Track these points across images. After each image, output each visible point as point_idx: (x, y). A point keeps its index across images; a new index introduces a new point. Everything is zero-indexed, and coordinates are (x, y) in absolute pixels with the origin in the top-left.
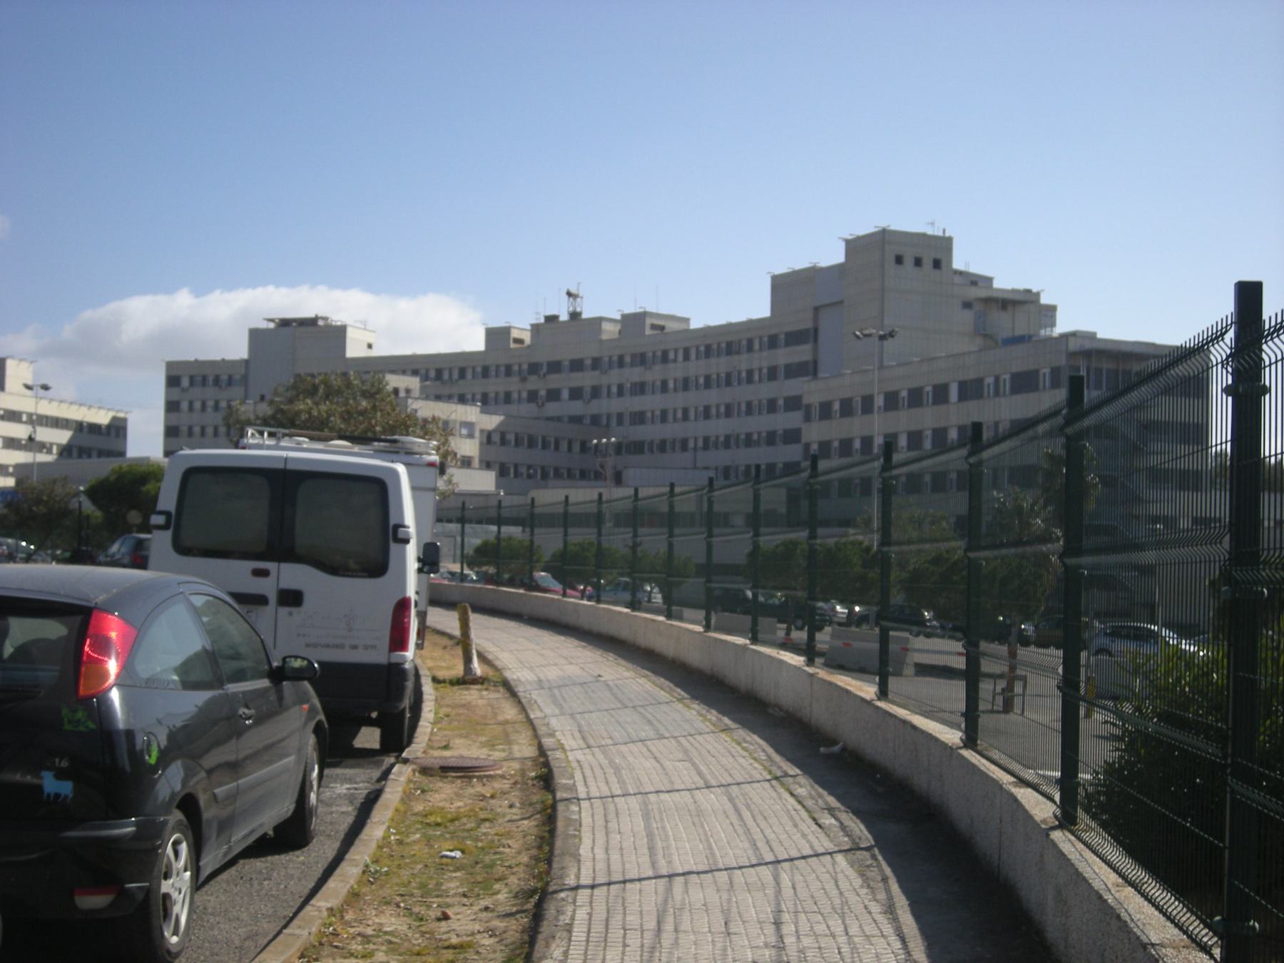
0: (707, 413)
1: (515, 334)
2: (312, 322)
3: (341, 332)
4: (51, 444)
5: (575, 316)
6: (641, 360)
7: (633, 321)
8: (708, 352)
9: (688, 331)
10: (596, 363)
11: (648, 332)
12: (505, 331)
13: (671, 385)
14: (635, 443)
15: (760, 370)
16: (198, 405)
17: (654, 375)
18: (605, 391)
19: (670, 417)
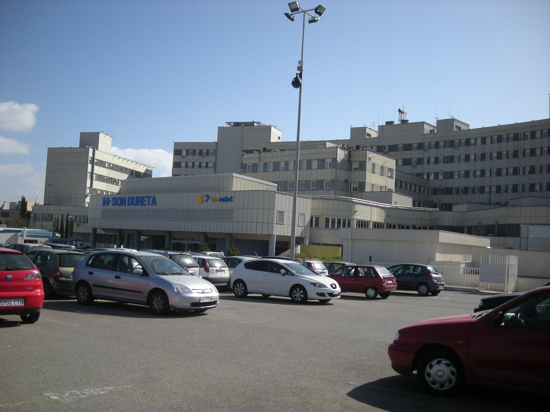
0: (499, 172)
1: (368, 131)
2: (252, 124)
3: (268, 129)
4: (119, 180)
5: (404, 122)
6: (451, 144)
7: (446, 125)
8: (500, 139)
9: (469, 130)
10: (420, 146)
11: (455, 129)
12: (363, 130)
13: (472, 157)
14: (447, 188)
15: (542, 149)
16: (190, 164)
17: (462, 151)
18: (426, 161)
19: (471, 175)
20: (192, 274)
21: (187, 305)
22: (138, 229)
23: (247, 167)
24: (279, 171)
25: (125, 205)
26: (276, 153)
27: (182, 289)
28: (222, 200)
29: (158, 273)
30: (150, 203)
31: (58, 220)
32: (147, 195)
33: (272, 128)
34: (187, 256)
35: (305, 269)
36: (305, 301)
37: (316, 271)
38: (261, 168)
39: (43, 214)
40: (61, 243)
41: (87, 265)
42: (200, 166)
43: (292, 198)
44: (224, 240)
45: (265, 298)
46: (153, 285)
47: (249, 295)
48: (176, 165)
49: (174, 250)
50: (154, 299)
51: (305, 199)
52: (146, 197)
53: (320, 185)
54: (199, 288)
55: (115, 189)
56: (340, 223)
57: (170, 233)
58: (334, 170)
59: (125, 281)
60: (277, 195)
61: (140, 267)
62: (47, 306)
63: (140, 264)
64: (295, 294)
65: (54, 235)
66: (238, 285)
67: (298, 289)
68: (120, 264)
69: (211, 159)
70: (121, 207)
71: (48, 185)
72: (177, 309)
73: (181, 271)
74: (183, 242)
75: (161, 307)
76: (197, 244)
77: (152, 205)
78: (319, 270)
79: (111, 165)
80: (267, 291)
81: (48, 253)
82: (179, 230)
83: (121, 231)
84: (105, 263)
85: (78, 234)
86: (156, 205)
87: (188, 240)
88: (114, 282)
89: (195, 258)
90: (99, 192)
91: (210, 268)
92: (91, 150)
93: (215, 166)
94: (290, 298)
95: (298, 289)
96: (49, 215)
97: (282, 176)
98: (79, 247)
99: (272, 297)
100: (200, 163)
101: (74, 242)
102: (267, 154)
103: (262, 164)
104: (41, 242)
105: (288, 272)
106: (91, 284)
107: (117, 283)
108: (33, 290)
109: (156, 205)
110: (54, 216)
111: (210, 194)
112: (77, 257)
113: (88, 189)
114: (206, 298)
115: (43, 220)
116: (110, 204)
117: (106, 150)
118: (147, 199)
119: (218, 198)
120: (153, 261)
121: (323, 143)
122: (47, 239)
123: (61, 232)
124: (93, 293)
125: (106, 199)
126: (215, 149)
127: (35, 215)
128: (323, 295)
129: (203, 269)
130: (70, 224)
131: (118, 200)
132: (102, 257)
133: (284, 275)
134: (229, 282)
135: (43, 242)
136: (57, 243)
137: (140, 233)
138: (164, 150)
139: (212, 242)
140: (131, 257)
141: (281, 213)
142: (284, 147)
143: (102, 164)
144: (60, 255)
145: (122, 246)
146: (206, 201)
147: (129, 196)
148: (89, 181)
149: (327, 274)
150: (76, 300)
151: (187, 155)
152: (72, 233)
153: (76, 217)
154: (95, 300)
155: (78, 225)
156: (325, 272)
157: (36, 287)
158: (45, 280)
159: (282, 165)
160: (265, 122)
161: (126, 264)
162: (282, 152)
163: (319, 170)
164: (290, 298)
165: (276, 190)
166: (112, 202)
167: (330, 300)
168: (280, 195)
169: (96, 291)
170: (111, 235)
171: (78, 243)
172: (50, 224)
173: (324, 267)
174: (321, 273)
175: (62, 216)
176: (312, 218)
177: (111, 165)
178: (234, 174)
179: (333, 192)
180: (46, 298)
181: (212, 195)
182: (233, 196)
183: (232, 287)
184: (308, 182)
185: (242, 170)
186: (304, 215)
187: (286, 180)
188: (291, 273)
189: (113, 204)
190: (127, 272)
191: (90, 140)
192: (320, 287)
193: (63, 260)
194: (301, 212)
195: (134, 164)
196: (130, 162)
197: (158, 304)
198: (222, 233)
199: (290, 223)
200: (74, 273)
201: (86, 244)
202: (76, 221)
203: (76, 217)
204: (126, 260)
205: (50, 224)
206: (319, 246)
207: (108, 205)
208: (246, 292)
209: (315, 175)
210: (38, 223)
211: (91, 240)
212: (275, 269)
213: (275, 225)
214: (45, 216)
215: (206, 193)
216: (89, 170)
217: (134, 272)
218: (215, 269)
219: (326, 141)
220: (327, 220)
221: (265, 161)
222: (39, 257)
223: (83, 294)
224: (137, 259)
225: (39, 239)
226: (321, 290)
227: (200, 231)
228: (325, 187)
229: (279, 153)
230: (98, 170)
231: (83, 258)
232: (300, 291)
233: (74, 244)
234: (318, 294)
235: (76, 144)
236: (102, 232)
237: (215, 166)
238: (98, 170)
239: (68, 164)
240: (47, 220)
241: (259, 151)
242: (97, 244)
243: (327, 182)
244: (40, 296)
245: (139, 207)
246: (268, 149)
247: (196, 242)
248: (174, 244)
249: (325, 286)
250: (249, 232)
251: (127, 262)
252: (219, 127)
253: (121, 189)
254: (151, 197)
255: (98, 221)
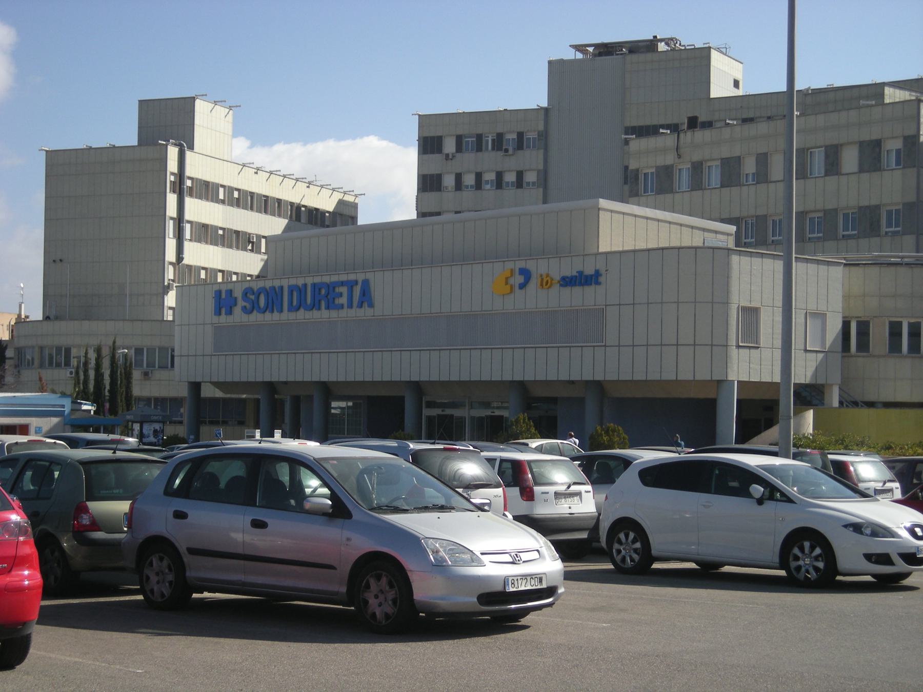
2: (650, 45)
4: (259, 237)
16: (469, 180)
20: (480, 508)
21: (468, 601)
22: (324, 379)
23: (641, 178)
24: (740, 185)
25: (281, 311)
26: (728, 129)
27: (451, 552)
28: (568, 282)
29: (380, 509)
30: (355, 303)
31: (86, 364)
32: (343, 278)
33: (714, 55)
34: (466, 455)
35: (827, 483)
36: (828, 580)
37: (862, 486)
38: (684, 179)
39: (42, 348)
40: (97, 431)
41: (169, 492)
42: (499, 183)
43: (779, 265)
44: (581, 401)
45: (708, 574)
46: (363, 544)
47: (656, 566)
48: (428, 183)
49: (431, 437)
50: (368, 586)
51: (823, 268)
52: (342, 284)
53: (867, 222)
54: (497, 547)
55: (249, 264)
56: (900, 334)
57: (417, 388)
58: (911, 172)
59: (283, 534)
60: (735, 258)
61: (325, 491)
62: (50, 617)
63: (325, 484)
64: (797, 558)
65: (76, 409)
66: (622, 536)
67: (807, 544)
68: (265, 485)
69: (531, 160)
70: (268, 316)
71: (54, 260)
72: (440, 614)
73: (448, 498)
74: (457, 413)
75: (389, 608)
76: (501, 418)
77: (360, 305)
78: (872, 485)
79: (236, 194)
80: (710, 552)
81: (55, 461)
82: (465, 377)
83: (271, 387)
84: (222, 485)
85: (148, 400)
86: (371, 305)
87: (472, 407)
88: (248, 538)
89: (491, 461)
90: (203, 275)
91: (537, 489)
92: (173, 152)
93: (544, 180)
94: (782, 573)
95: (807, 544)
96: (59, 349)
97: (750, 199)
98: (152, 439)
99: (727, 569)
100: (500, 175)
101: (137, 427)
102: (700, 135)
103: (686, 166)
104: (38, 431)
105: (773, 493)
106: (182, 547)
107: (259, 542)
108: (8, 571)
109: (371, 305)
110: (74, 352)
111: (531, 265)
112: (143, 467)
113: (171, 268)
114: (524, 577)
115: (42, 366)
116: (237, 310)
117: (217, 147)
118: (344, 290)
119: (557, 278)
120: (363, 472)
121: (875, 91)
122: (55, 420)
123: (96, 399)
124: (188, 574)
125: (225, 296)
126: (541, 127)
127: (20, 351)
128: (884, 559)
129: (516, 491)
130: (122, 374)
131: (260, 296)
132: (213, 467)
133: (760, 502)
134: (595, 529)
135: (45, 429)
136: (87, 431)
137: (328, 390)
138: (383, 137)
139: (545, 410)
140: (296, 462)
141: (751, 314)
142: (750, 110)
143: (206, 190)
144: (87, 464)
145: (278, 434)
146: (522, 286)
147: (293, 282)
148: (171, 245)
149: (898, 494)
150: (141, 597)
151: (451, 149)
152: (129, 400)
153: (139, 351)
154: (195, 595)
155: (146, 374)
156: (890, 490)
157: (17, 562)
158: (45, 542)
159: (750, 166)
160: (690, 39)
161: (281, 484)
162: (746, 127)
163: (865, 176)
164: (782, 573)
165: (731, 244)
166: (241, 303)
167: (906, 575)
168: (745, 260)
169: (196, 569)
170: (244, 400)
171: (148, 429)
172: (64, 375)
173: (888, 474)
174: (878, 492)
175: (98, 350)
176: (846, 325)
177: (236, 194)
178: (603, 203)
179: (909, 240)
180: (48, 593)
181: (539, 267)
182: (603, 271)
183: (603, 543)
184: (830, 215)
185: (626, 187)
186: (821, 316)
187: (761, 212)
188: (783, 494)
189: (244, 309)
190: (287, 508)
191: (168, 122)
192: (874, 534)
193: (98, 479)
194: (812, 307)
195: (301, 186)
196: (277, 179)
197: (380, 598)
198: (573, 382)
199: (778, 342)
200: (130, 517)
201: (170, 430)
202: (139, 364)
203: (139, 351)
204: (284, 473)
205: (64, 375)
206: (872, 411)
207: (230, 312)
208: (647, 555)
209: (852, 190)
210: (28, 375)
211: (185, 419)
212: (735, 484)
213: (734, 352)
214: (47, 352)
215: (522, 264)
216: (171, 209)
217: (307, 506)
218: (552, 489)
219: (883, 84)
220: (895, 330)
221: (696, 158)
222: (29, 474)
223: (160, 580)
224: (315, 467)
225: (34, 422)
226: (878, 546)
227: (508, 377)
228: (884, 229)
229: (738, 129)
230: (198, 210)
231: (156, 471)
232: (812, 548)
233: (136, 432)
234: (869, 557)
235: (126, 134)
236: (219, 394)
237: (544, 180)
238: (198, 210)
239: (106, 199)
240: (52, 363)
241: (675, 128)
242: (204, 429)
243: (889, 213)
244: (29, 588)
245: (324, 314)
246: (702, 119)
247: (498, 413)
248: (430, 419)
249: (892, 534)
250: (654, 376)
251: (286, 479)
252: (550, 62)
253: (266, 262)
254: (356, 282)
255: (203, 361)
